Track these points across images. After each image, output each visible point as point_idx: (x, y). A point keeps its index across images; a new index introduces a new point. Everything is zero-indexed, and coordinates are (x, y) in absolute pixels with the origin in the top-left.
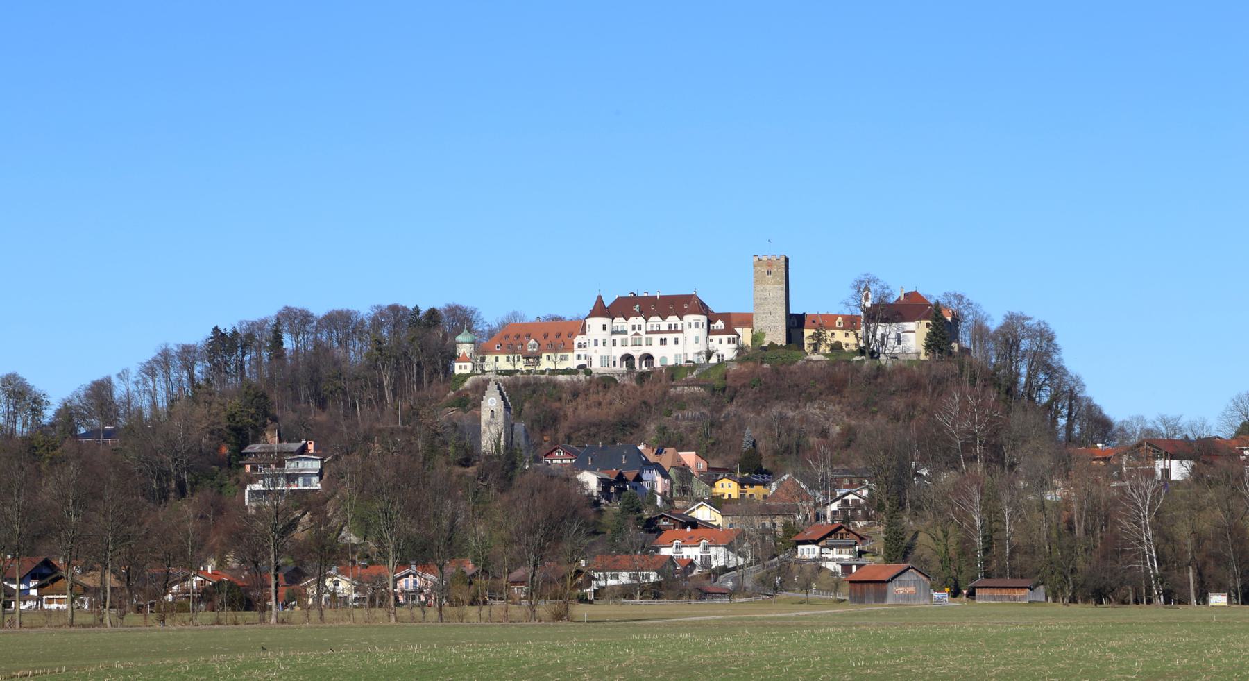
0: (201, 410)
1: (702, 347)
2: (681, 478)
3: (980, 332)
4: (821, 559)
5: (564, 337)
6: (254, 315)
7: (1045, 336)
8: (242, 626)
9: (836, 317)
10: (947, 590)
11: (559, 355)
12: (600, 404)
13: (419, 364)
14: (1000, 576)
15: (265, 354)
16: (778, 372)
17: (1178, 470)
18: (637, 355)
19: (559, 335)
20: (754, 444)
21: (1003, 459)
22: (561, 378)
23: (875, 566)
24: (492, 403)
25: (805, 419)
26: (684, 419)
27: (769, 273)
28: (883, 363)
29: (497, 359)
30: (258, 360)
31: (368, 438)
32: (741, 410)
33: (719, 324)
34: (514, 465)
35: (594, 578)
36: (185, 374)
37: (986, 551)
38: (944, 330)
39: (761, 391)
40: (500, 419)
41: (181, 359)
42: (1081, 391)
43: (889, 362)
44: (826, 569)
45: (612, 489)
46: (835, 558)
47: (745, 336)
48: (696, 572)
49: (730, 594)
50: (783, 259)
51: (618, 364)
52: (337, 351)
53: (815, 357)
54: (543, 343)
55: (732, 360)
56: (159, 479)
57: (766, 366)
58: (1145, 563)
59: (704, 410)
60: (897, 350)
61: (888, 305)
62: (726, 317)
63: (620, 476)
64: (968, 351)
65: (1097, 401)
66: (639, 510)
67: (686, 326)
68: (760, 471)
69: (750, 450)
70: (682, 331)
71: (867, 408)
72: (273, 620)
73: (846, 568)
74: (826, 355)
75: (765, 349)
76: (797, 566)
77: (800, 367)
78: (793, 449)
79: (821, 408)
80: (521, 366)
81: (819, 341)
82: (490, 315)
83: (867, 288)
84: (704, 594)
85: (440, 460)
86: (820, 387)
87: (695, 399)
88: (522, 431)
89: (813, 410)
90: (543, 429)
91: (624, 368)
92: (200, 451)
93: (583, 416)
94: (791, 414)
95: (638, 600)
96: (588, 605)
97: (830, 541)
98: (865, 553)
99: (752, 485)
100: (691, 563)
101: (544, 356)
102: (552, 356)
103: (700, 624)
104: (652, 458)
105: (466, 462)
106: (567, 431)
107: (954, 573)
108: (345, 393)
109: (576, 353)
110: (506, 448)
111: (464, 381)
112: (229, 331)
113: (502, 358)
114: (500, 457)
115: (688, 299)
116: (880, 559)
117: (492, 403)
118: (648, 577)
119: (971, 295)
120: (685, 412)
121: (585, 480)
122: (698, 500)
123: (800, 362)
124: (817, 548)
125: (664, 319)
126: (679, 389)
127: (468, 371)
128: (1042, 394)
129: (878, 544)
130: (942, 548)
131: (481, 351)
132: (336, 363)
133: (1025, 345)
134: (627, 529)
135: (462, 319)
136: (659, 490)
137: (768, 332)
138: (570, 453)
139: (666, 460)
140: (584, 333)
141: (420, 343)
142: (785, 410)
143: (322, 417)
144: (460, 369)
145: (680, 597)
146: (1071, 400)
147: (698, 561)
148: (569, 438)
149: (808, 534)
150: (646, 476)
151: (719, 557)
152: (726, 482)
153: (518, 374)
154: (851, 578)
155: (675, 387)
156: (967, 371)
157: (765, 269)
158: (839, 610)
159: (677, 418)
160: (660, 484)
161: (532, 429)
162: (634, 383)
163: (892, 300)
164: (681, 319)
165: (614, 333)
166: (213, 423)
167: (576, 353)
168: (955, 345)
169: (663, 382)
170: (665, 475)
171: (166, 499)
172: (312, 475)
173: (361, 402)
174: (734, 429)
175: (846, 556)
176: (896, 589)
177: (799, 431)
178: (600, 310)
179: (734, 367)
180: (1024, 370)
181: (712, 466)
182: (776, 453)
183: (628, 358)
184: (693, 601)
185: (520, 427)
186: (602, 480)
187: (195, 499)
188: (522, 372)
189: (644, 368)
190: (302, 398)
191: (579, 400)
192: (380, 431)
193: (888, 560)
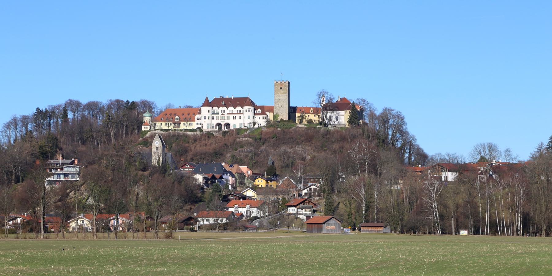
0: (27, 145)
1: (251, 120)
2: (240, 178)
3: (372, 116)
4: (297, 213)
5: (191, 115)
6: (55, 103)
7: (400, 118)
8: (28, 239)
9: (310, 108)
10: (350, 227)
11: (188, 123)
12: (206, 145)
13: (126, 126)
14: (372, 222)
15: (60, 120)
16: (284, 132)
17: (451, 176)
18: (223, 124)
19: (189, 114)
20: (273, 163)
21: (377, 171)
22: (189, 133)
23: (319, 217)
24: (157, 143)
25: (295, 153)
26: (242, 152)
27: (281, 88)
28: (330, 128)
29: (161, 124)
30: (57, 122)
31: (101, 158)
32: (268, 148)
33: (259, 111)
34: (165, 171)
35: (199, 221)
36: (24, 128)
37: (366, 211)
38: (356, 114)
39: (276, 140)
40: (160, 150)
41: (22, 121)
42: (415, 142)
43: (332, 128)
44: (299, 218)
45: (209, 182)
46: (303, 213)
47: (270, 116)
48: (244, 218)
49: (257, 228)
50: (287, 83)
51: (214, 127)
52: (92, 120)
53: (300, 126)
54: (182, 118)
55: (264, 126)
56: (7, 174)
57: (279, 129)
58: (434, 217)
59: (252, 148)
60: (336, 123)
61: (333, 104)
62: (262, 108)
63: (213, 176)
64: (367, 124)
65: (422, 146)
66: (220, 191)
67: (245, 111)
68: (275, 175)
69: (271, 166)
70: (243, 113)
71: (323, 148)
72: (42, 237)
73: (308, 217)
74: (305, 125)
75: (279, 122)
76: (287, 217)
77: (294, 130)
78: (289, 166)
79: (302, 148)
80: (172, 127)
81: (302, 118)
82: (160, 104)
83: (323, 96)
84: (245, 228)
85: (133, 169)
86: (302, 139)
87: (248, 143)
88: (170, 156)
89: (299, 149)
90: (181, 155)
91: (217, 129)
92: (27, 162)
93: (198, 150)
94: (289, 150)
95: (217, 231)
96: (195, 233)
97: (301, 206)
98: (316, 211)
99: (271, 181)
100: (242, 215)
101: (182, 123)
102: (186, 123)
103: (228, 241)
104: (228, 169)
105: (144, 169)
106: (191, 156)
107: (354, 220)
108: (93, 138)
109: (196, 122)
110: (162, 163)
111: (146, 134)
112: (44, 110)
113: (164, 124)
114: (159, 167)
115: (245, 99)
116: (323, 214)
117: (157, 143)
118: (222, 220)
119: (368, 100)
120: (243, 149)
121: (197, 178)
122: (247, 187)
123: (294, 128)
124: (296, 209)
125: (235, 108)
126: (241, 139)
127: (148, 129)
128: (398, 143)
129: (322, 208)
130: (348, 210)
131: (154, 120)
132: (91, 125)
133: (391, 121)
134: (215, 199)
135: (148, 106)
136: (231, 183)
138: (192, 166)
139: (234, 170)
140: (200, 113)
141: (127, 117)
142: (287, 149)
143: (83, 149)
144: (144, 128)
145: (235, 229)
146: (410, 146)
147: (245, 214)
148: (192, 159)
149: (292, 203)
150: (225, 176)
151: (255, 212)
152: (260, 179)
153: (170, 131)
154: (309, 221)
155: (239, 138)
156: (366, 133)
158: (303, 235)
159: (240, 151)
160: (231, 180)
161: (176, 155)
162: (221, 136)
163: (334, 101)
164: (242, 108)
165: (213, 114)
166: (33, 151)
167: (196, 122)
168: (361, 121)
169: (234, 135)
170: (233, 176)
171: (11, 183)
172: (75, 174)
173: (101, 142)
174: (264, 157)
175: (308, 212)
176: (326, 227)
177: (293, 158)
178: (207, 103)
179: (265, 129)
180: (390, 133)
181: (254, 172)
182: (282, 167)
183: (219, 125)
184: (241, 231)
185: (169, 154)
186: (205, 178)
187: (24, 183)
188: (172, 130)
189: (226, 129)
190: (76, 140)
191: (197, 142)
192: (106, 155)
193: (325, 215)
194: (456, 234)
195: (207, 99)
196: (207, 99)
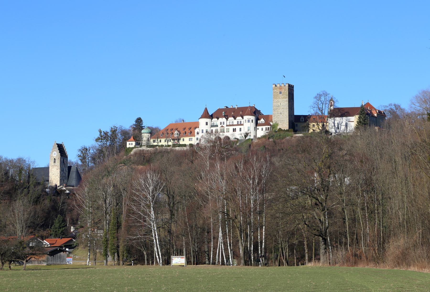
27: (280, 93)
70: (243, 125)
101: (182, 139)
109: (196, 137)
113: (163, 140)
125: (235, 119)
127: (133, 146)
137: (280, 123)
153: (157, 147)
157: (278, 91)
164: (227, 119)
165: (212, 126)
167: (196, 137)
178: (206, 115)
195: (206, 110)
196: (206, 110)
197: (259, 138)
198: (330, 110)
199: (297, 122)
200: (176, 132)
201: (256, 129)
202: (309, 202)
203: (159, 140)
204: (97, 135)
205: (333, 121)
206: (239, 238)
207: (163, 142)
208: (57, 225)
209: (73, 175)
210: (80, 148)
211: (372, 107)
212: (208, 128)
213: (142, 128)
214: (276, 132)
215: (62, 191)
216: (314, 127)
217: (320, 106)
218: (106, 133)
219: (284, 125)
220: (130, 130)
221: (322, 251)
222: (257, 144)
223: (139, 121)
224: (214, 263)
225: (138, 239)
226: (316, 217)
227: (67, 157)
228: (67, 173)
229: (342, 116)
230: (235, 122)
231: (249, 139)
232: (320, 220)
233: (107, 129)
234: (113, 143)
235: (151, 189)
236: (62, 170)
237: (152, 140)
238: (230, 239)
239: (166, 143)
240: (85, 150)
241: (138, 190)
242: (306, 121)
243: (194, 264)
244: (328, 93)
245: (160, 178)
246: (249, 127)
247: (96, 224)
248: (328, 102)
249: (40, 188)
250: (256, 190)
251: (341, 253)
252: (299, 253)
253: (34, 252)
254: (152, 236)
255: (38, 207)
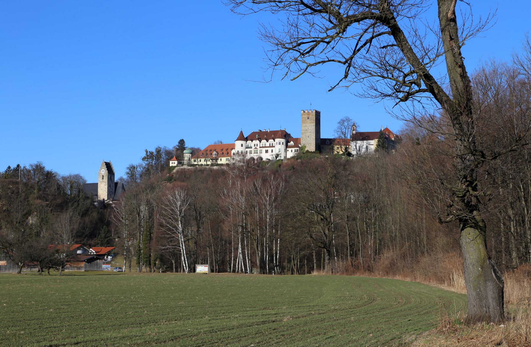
27: (308, 118)
70: (274, 147)
101: (219, 159)
113: (203, 160)
127: (175, 165)
153: (197, 166)
157: (306, 116)
164: (260, 142)
165: (247, 148)
178: (241, 137)
194: (190, 271)
197: (288, 159)
198: (353, 134)
199: (322, 144)
200: (215, 153)
201: (286, 151)
202: (316, 218)
203: (199, 160)
204: (144, 155)
205: (355, 144)
206: (256, 249)
207: (203, 162)
208: (103, 235)
209: (119, 190)
210: (128, 166)
211: (390, 132)
212: (242, 149)
213: (184, 149)
214: (304, 153)
215: (109, 205)
216: (339, 150)
217: (344, 131)
218: (152, 153)
219: (311, 147)
220: (173, 151)
221: (327, 261)
222: (287, 164)
223: (182, 142)
224: (234, 271)
225: (167, 249)
226: (322, 231)
227: (113, 174)
228: (114, 189)
229: (363, 139)
230: (268, 144)
231: (279, 160)
232: (325, 233)
233: (152, 149)
234: (158, 160)
235: (179, 204)
236: (109, 186)
237: (193, 160)
238: (248, 250)
239: (205, 163)
240: (132, 168)
241: (167, 206)
242: (331, 144)
243: (216, 272)
244: (350, 118)
245: (187, 194)
246: (279, 149)
247: (132, 236)
248: (350, 127)
249: (89, 201)
250: (272, 205)
251: (341, 263)
252: (307, 264)
253: (69, 260)
254: (180, 246)
255: (87, 219)
